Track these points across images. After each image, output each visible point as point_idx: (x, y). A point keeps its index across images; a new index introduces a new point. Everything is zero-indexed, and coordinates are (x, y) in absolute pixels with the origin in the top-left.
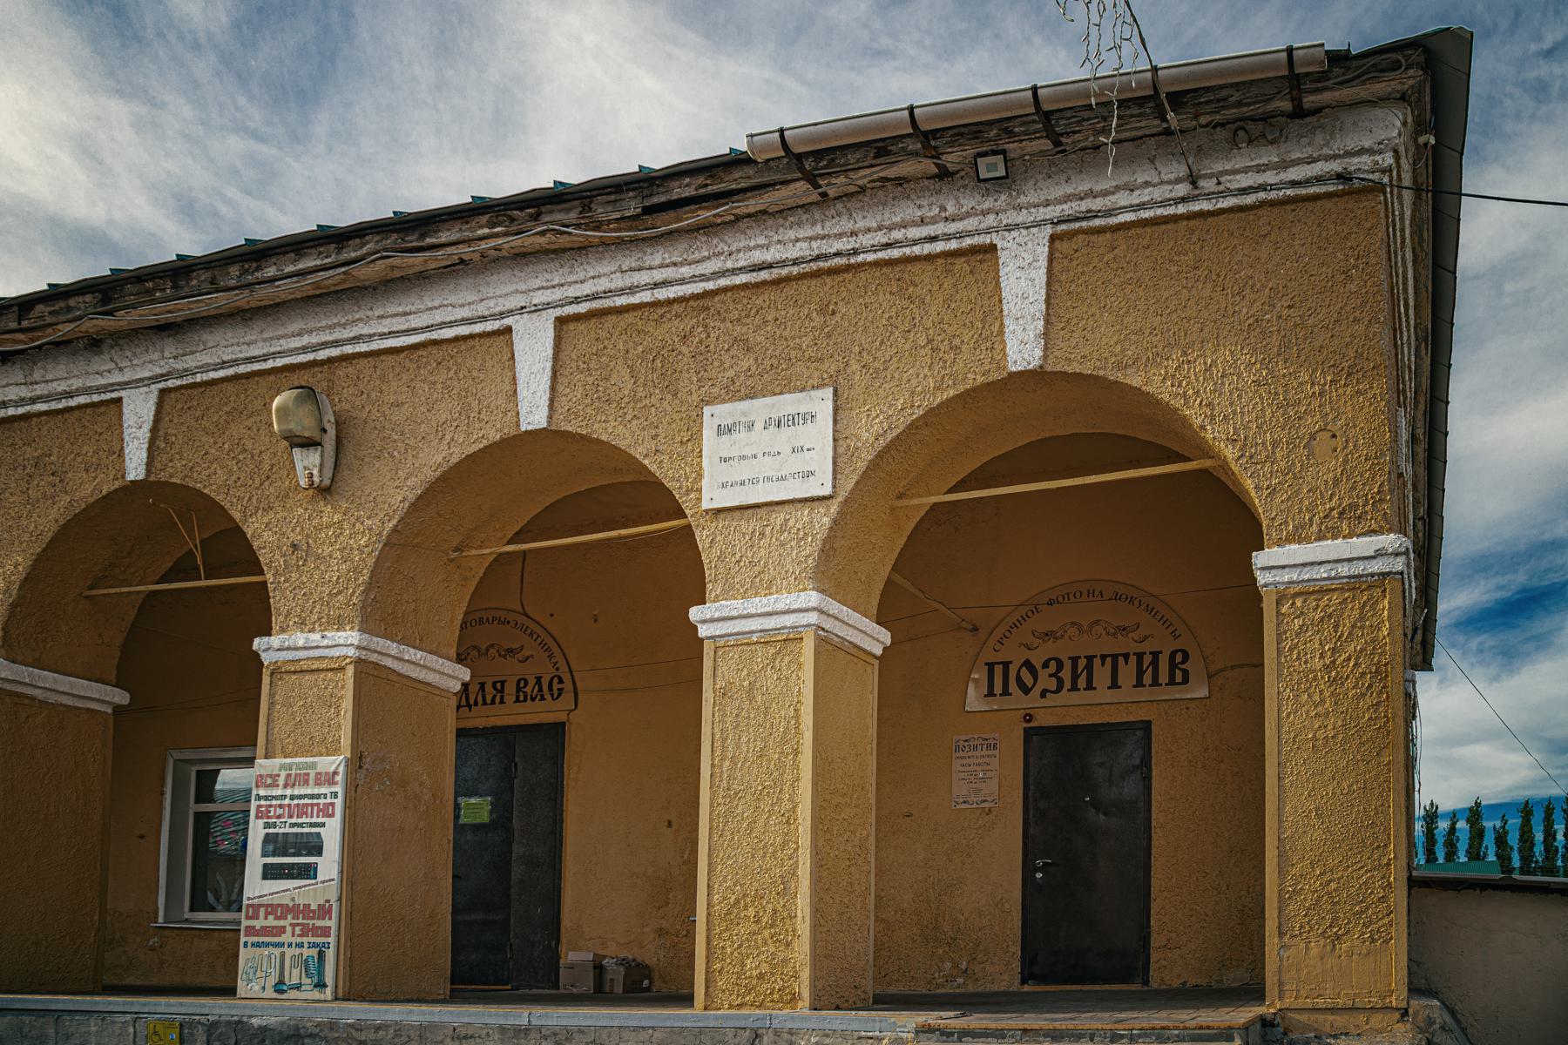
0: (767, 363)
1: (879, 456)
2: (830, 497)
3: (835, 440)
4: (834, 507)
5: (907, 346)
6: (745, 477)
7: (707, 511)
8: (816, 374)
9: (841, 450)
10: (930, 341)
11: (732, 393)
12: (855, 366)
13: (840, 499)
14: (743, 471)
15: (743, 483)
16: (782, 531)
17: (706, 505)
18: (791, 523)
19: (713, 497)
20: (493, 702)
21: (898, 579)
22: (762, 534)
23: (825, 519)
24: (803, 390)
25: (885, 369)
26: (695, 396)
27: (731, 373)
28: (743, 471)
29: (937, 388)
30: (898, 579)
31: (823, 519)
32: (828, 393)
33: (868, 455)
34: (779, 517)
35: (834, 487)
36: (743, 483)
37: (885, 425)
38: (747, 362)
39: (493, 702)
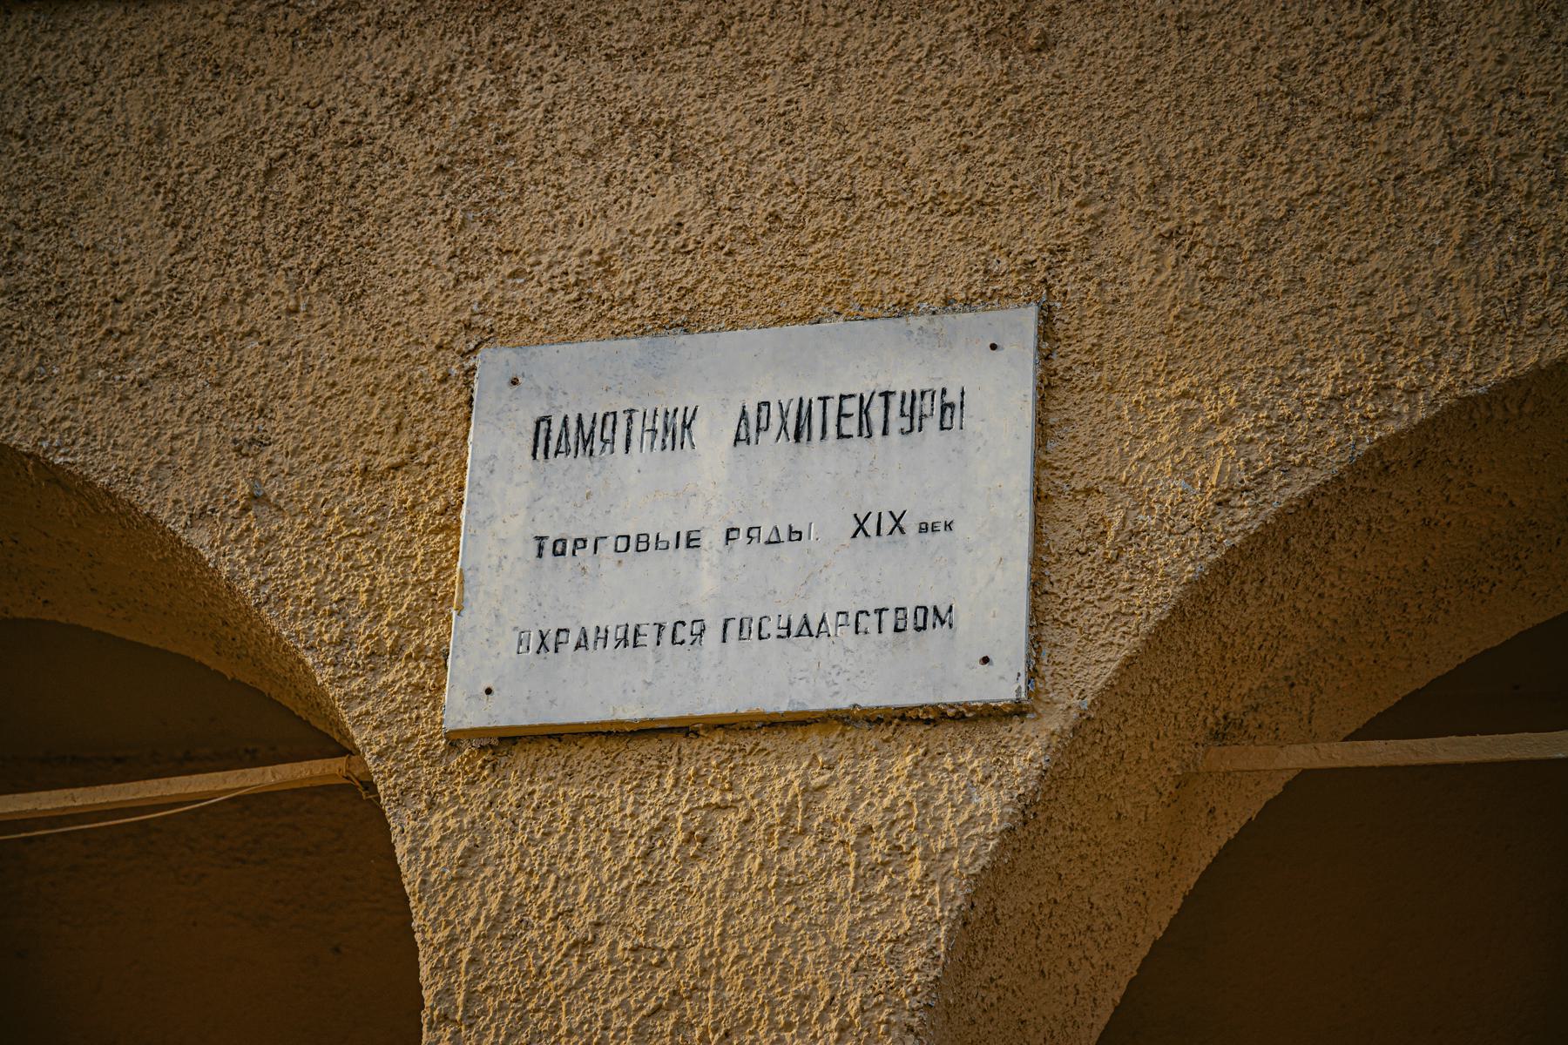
0: (756, 207)
1: (1224, 569)
2: (1017, 711)
3: (1040, 498)
4: (1028, 753)
5: (1363, 170)
6: (645, 617)
7: (455, 740)
8: (963, 256)
9: (1061, 537)
10: (1459, 157)
11: (594, 304)
12: (1127, 234)
13: (1055, 722)
14: (617, 593)
15: (631, 638)
16: (789, 834)
17: (463, 709)
18: (835, 801)
19: (487, 679)
20: (923, 393)
21: (332, 768)
22: (700, 840)
23: (984, 797)
24: (903, 309)
25: (1265, 250)
26: (435, 311)
27: (599, 236)
28: (617, 593)
29: (1490, 327)
30: (332, 768)
31: (977, 798)
32: (1028, 318)
33: (1178, 563)
34: (783, 774)
35: (1033, 674)
36: (631, 638)
37: (1262, 456)
38: (678, 197)
39: (923, 393)
